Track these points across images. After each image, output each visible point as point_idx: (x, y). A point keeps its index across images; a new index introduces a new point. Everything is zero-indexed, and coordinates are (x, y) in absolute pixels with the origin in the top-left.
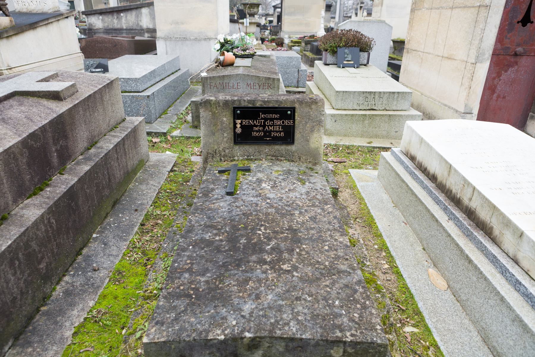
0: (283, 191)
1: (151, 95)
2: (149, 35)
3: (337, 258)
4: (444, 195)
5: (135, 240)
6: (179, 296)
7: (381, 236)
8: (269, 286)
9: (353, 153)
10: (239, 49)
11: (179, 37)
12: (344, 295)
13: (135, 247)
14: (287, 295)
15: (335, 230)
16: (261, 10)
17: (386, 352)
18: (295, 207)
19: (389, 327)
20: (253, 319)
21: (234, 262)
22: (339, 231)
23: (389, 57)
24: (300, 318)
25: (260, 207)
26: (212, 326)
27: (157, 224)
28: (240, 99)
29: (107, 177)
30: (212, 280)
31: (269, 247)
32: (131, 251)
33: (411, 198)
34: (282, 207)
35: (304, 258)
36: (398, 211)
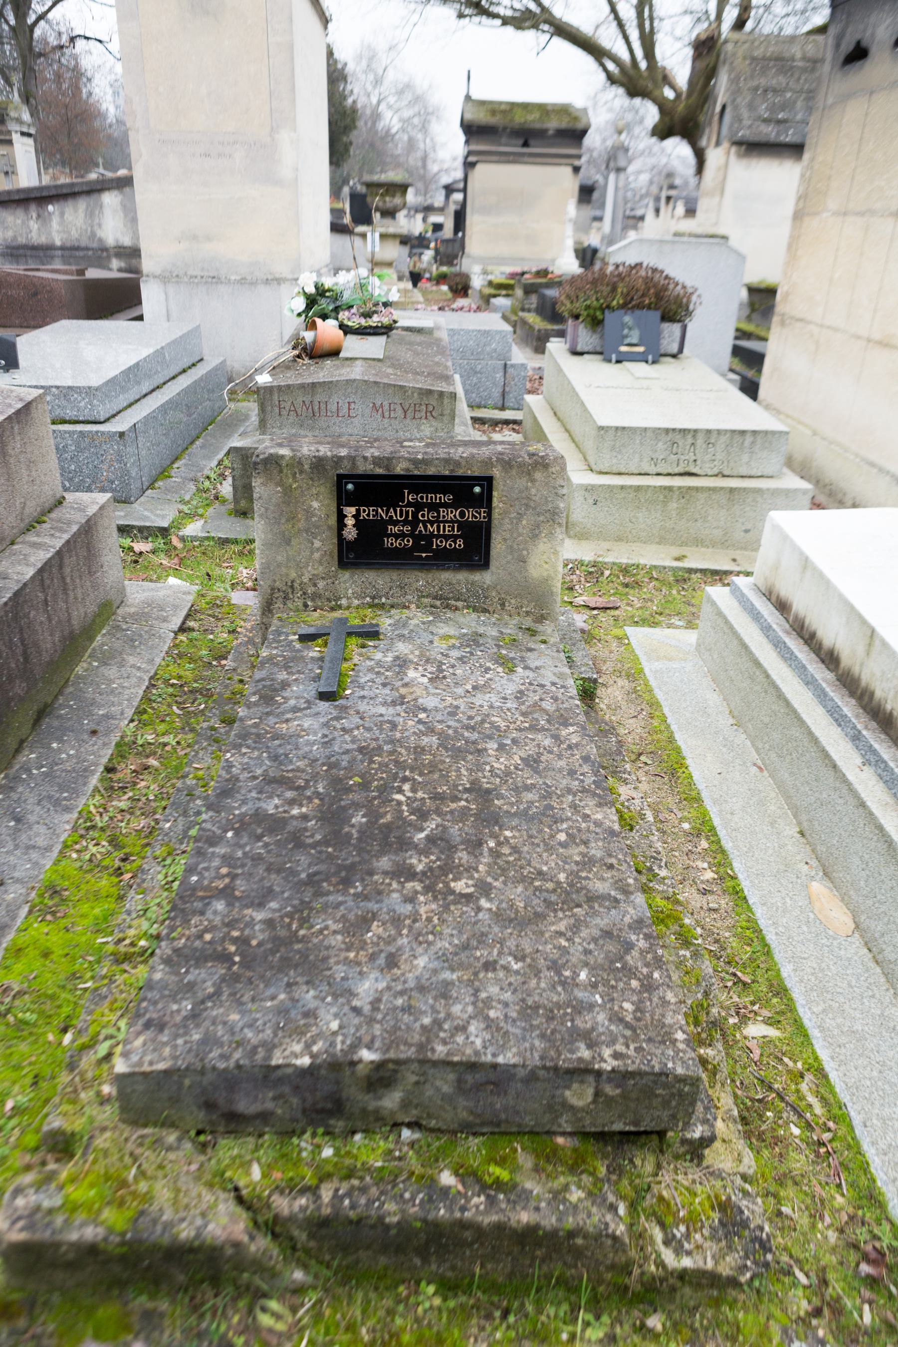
0: (460, 691)
1: (130, 430)
2: (123, 265)
3: (588, 862)
4: (853, 702)
5: (92, 808)
6: (200, 958)
7: (698, 799)
8: (419, 934)
9: (638, 584)
10: (354, 310)
11: (199, 273)
12: (599, 956)
13: (93, 827)
14: (463, 956)
15: (584, 791)
16: (411, 197)
17: (697, 1093)
18: (488, 732)
19: (708, 1028)
20: (379, 1017)
21: (336, 873)
22: (594, 795)
23: (738, 330)
24: (492, 1014)
25: (402, 731)
26: (280, 1034)
27: (146, 768)
28: (353, 454)
29: (19, 651)
30: (282, 917)
31: (422, 835)
32: (82, 836)
33: (775, 707)
34: (456, 731)
35: (508, 862)
36: (744, 736)
